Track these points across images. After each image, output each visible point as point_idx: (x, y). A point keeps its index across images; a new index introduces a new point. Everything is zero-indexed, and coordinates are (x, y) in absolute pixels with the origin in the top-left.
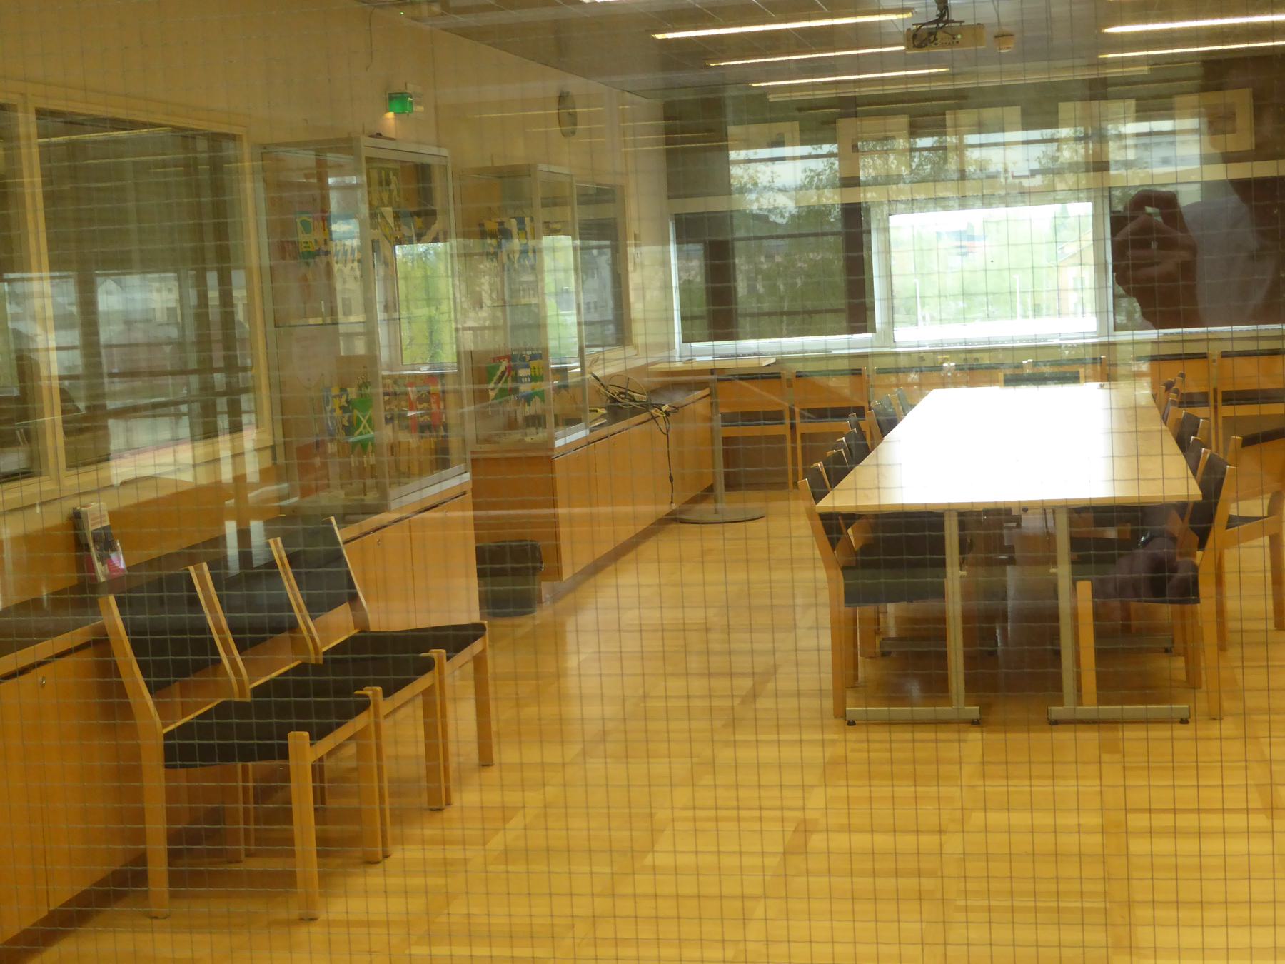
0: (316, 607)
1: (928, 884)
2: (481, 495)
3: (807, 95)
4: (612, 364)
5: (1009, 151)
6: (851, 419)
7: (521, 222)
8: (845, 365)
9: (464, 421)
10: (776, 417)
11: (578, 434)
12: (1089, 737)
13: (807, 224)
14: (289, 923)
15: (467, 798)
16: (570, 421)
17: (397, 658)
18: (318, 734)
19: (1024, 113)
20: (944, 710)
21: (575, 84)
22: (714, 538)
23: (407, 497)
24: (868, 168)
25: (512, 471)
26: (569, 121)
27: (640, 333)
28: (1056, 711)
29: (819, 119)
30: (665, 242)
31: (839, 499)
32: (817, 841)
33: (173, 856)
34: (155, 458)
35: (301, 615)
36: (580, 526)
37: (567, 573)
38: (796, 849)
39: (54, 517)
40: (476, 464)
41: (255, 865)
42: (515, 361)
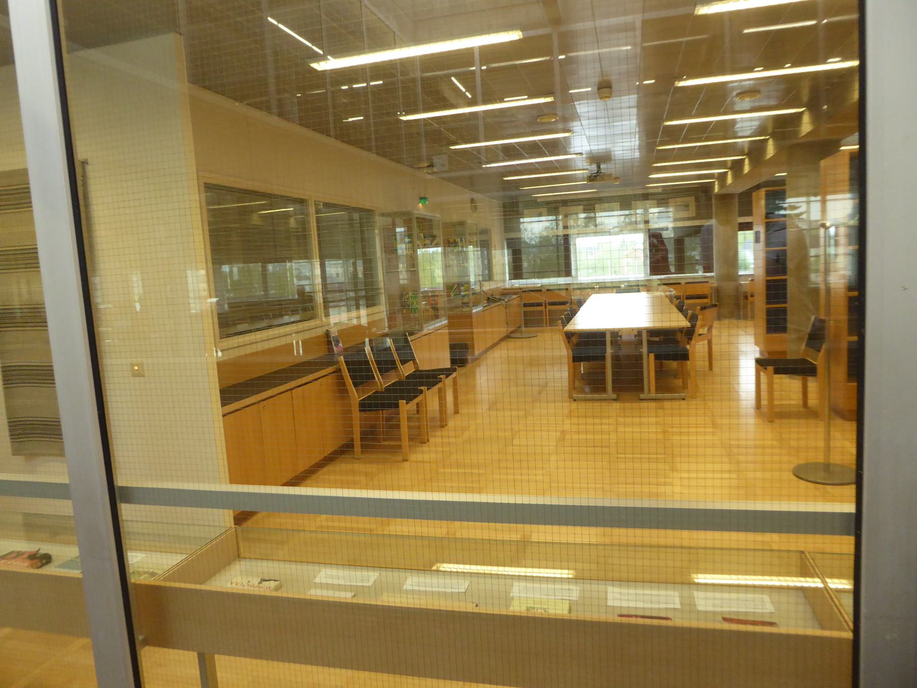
0: (404, 362)
1: (606, 450)
2: (450, 326)
3: (551, 199)
4: (488, 286)
5: (610, 218)
6: (566, 304)
7: (461, 241)
8: (564, 287)
9: (442, 302)
10: (540, 305)
11: (479, 309)
12: (653, 405)
13: (544, 242)
14: (398, 462)
15: (451, 423)
16: (476, 304)
17: (431, 378)
18: (409, 400)
19: (621, 205)
20: (604, 396)
21: (476, 196)
22: (518, 343)
23: (429, 327)
24: (571, 222)
25: (460, 319)
26: (475, 208)
27: (497, 277)
28: (642, 396)
29: (553, 207)
30: (503, 249)
31: (570, 327)
32: (568, 436)
33: (362, 439)
34: (339, 318)
35: (398, 363)
36: (482, 337)
37: (477, 353)
38: (562, 439)
39: (320, 332)
40: (450, 318)
41: (386, 443)
42: (460, 285)
